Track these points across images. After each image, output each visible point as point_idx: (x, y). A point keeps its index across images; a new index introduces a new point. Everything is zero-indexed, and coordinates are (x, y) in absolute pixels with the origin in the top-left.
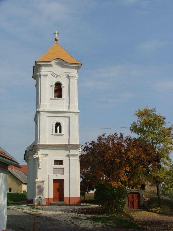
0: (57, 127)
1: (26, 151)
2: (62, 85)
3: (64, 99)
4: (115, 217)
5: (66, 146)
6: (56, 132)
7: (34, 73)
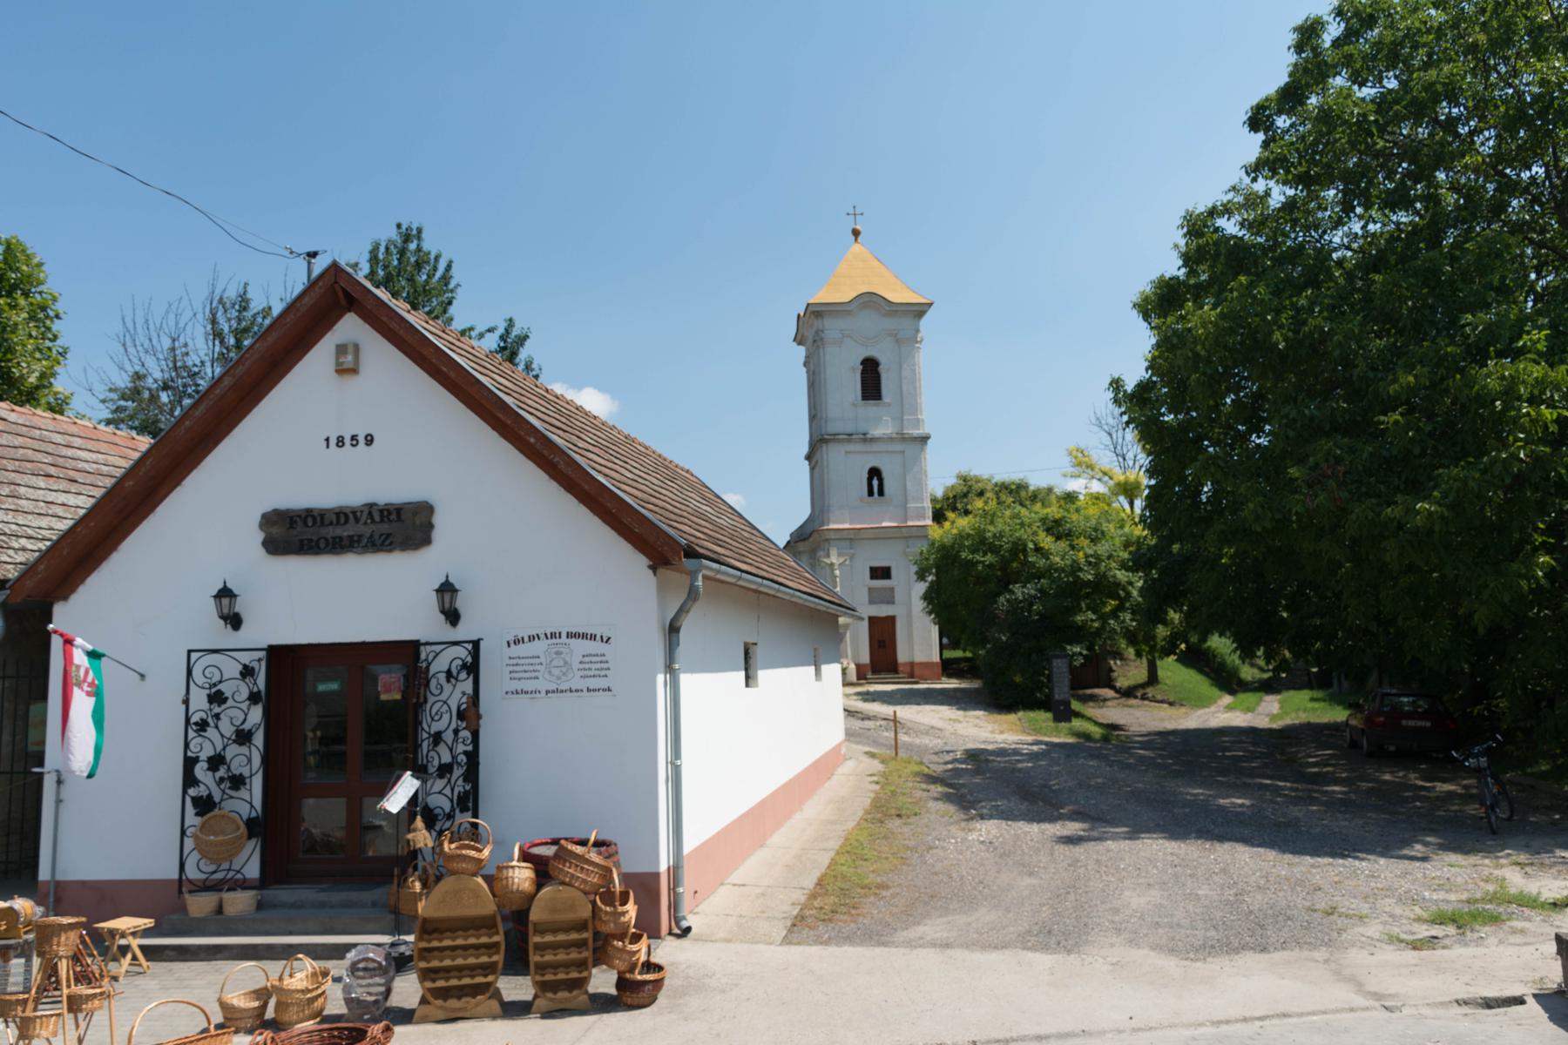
3: (889, 405)
6: (871, 493)
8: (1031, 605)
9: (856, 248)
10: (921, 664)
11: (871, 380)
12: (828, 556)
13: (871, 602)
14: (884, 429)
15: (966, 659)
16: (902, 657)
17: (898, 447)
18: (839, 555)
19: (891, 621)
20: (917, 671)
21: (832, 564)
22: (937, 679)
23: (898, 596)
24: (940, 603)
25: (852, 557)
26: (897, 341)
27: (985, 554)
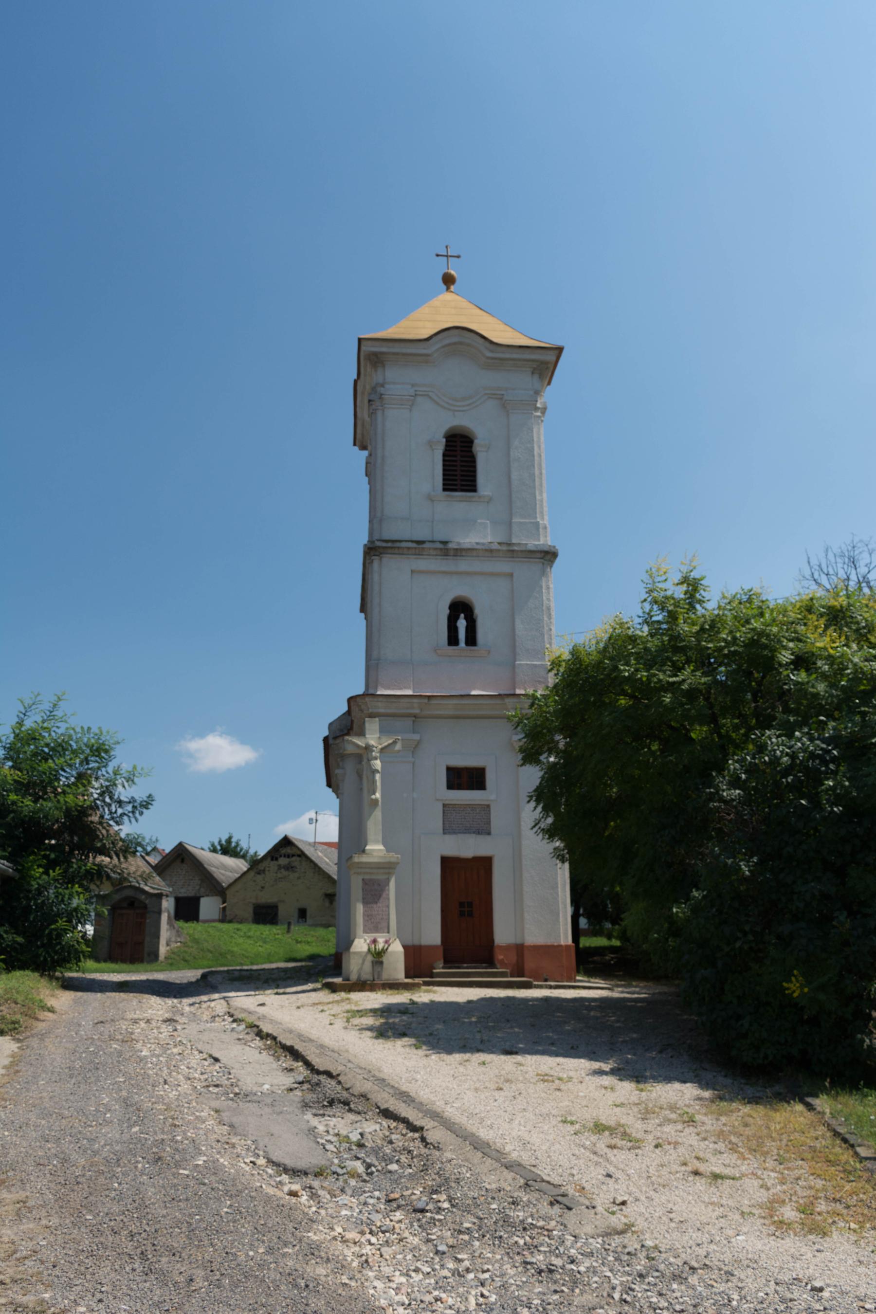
0: (458, 618)
1: (326, 740)
2: (476, 442)
3: (490, 500)
4: (104, 832)
5: (498, 701)
6: (453, 640)
7: (359, 414)
8: (815, 777)
9: (448, 296)
10: (537, 948)
11: (460, 464)
12: (362, 733)
13: (448, 829)
14: (481, 534)
15: (612, 949)
16: (503, 934)
17: (503, 566)
18: (383, 731)
19: (483, 866)
20: (530, 964)
21: (368, 748)
22: (565, 979)
23: (497, 821)
24: (575, 813)
25: (415, 748)
26: (504, 406)
27: (677, 669)
